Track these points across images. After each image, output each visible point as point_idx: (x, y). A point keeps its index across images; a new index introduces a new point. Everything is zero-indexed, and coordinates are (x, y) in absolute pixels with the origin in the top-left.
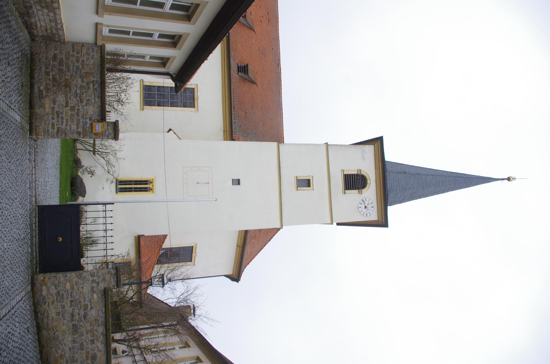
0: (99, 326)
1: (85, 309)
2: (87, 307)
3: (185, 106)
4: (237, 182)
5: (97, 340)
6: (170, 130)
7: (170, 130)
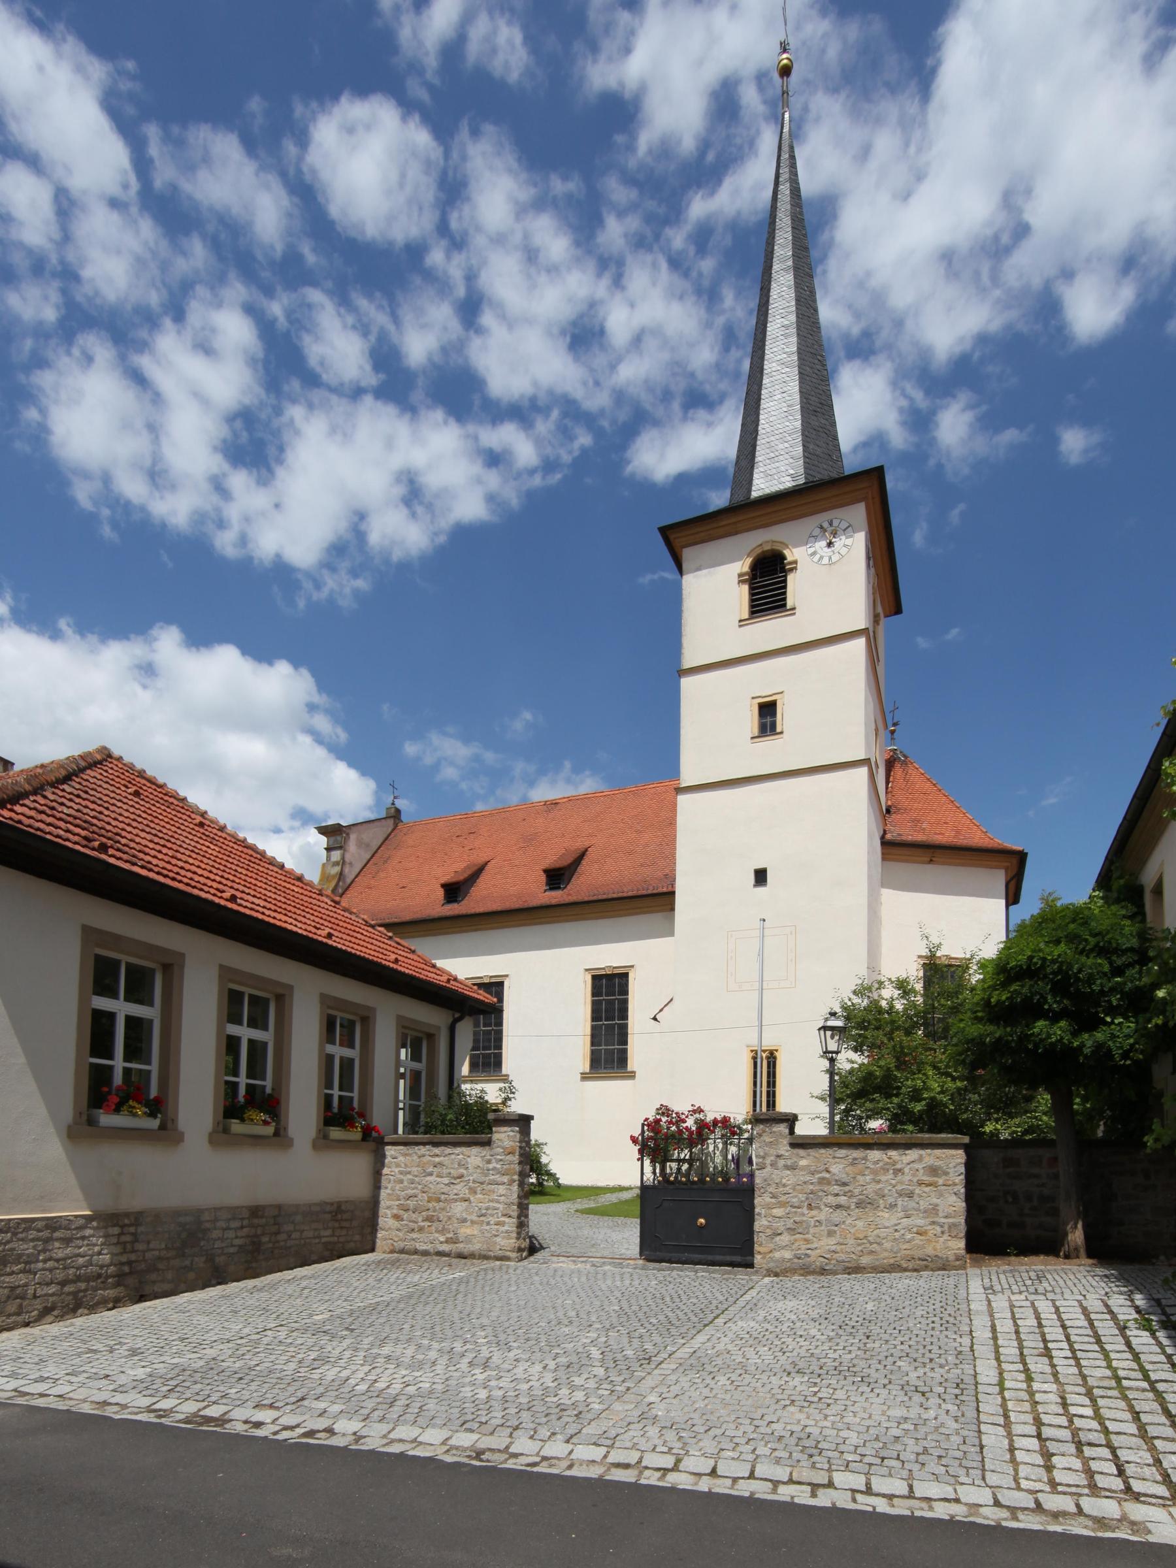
0: (865, 1158)
1: (829, 1183)
2: (824, 1178)
3: (624, 991)
4: (761, 877)
5: (895, 1163)
6: (655, 1019)
7: (655, 1019)
